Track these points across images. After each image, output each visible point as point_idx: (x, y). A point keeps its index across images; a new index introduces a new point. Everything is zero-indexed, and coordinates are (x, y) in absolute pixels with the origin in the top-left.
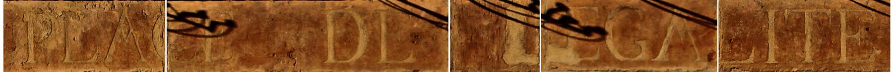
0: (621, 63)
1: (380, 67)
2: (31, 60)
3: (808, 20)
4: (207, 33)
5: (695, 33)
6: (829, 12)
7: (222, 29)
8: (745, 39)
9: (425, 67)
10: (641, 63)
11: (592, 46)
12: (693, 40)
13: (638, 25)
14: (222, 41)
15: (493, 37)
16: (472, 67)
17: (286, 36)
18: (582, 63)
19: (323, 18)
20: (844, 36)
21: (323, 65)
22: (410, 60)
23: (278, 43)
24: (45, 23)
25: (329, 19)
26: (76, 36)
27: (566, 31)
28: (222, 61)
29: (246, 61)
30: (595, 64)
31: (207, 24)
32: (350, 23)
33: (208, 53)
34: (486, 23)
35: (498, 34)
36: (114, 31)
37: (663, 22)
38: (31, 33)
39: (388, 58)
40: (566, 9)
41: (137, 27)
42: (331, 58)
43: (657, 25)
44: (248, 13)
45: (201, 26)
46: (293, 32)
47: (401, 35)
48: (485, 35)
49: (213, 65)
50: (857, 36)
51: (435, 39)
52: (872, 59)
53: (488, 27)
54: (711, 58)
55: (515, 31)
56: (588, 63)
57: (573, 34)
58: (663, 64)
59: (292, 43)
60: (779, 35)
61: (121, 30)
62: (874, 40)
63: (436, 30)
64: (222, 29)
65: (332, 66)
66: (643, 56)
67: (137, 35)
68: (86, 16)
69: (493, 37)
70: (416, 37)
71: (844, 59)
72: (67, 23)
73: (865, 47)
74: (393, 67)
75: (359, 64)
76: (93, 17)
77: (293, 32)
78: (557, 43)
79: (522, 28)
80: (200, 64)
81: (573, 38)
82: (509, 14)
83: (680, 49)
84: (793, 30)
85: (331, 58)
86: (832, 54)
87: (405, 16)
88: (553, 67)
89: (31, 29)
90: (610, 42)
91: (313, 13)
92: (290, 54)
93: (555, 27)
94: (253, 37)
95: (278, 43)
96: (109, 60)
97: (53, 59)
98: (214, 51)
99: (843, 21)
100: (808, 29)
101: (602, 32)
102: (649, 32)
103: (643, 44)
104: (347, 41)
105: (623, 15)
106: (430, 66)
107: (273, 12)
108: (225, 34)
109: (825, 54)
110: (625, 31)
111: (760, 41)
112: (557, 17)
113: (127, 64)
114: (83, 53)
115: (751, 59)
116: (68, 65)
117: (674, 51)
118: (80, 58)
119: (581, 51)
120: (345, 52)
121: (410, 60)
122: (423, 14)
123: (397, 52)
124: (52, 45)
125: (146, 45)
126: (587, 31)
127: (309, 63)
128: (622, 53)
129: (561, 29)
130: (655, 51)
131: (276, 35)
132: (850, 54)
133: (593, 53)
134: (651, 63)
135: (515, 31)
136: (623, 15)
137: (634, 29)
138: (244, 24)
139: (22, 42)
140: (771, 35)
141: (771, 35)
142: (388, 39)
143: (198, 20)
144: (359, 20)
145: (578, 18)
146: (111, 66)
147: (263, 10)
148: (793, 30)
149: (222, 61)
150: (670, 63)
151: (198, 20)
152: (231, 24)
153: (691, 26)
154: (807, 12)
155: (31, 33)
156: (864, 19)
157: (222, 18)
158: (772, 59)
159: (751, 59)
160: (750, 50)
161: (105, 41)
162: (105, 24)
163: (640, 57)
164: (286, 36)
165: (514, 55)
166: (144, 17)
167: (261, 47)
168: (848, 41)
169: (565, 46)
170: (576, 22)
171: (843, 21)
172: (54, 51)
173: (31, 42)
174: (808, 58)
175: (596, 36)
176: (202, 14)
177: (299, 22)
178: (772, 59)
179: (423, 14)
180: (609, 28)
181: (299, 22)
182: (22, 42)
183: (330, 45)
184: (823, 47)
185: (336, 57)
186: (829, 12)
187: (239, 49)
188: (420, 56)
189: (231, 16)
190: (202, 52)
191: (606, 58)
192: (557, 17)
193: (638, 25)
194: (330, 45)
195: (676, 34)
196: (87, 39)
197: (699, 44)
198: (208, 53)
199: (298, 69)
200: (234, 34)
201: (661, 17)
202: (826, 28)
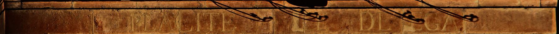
0: (430, 32)
1: (379, 32)
2: (133, 30)
3: (211, 16)
4: (318, 20)
5: (456, 21)
6: (218, 14)
7: (323, 19)
8: (189, 23)
9: (395, 32)
10: (437, 31)
11: (419, 25)
12: (455, 23)
13: (436, 18)
14: (323, 23)
15: (288, 22)
16: (280, 32)
17: (346, 21)
18: (416, 31)
19: (359, 15)
20: (224, 22)
21: (359, 31)
22: (389, 29)
23: (343, 23)
24: (137, 17)
25: (361, 15)
26: (148, 22)
27: (410, 20)
28: (323, 30)
29: (332, 30)
30: (421, 32)
31: (318, 17)
32: (368, 16)
33: (318, 27)
34: (285, 17)
35: (289, 21)
36: (162, 20)
37: (445, 17)
38: (133, 21)
39: (382, 29)
40: (410, 13)
41: (170, 19)
42: (361, 29)
43: (442, 18)
44: (333, 13)
45: (316, 18)
46: (348, 20)
47: (386, 21)
48: (285, 22)
49: (320, 31)
50: (228, 22)
51: (398, 22)
52: (234, 30)
53: (286, 19)
54: (461, 29)
55: (295, 20)
56: (418, 32)
57: (413, 21)
58: (444, 32)
59: (348, 24)
60: (201, 22)
61: (164, 19)
62: (234, 23)
63: (399, 19)
64: (323, 19)
65: (362, 31)
66: (437, 29)
67: (170, 21)
68: (152, 14)
69: (288, 22)
70: (391, 21)
71: (224, 30)
72: (145, 17)
73: (231, 26)
74: (383, 32)
75: (372, 31)
76: (154, 15)
77: (348, 20)
78: (407, 24)
79: (298, 19)
80: (316, 31)
81: (413, 23)
82: (293, 14)
83: (451, 27)
84: (206, 20)
85: (361, 29)
86: (220, 28)
87: (388, 14)
88: (406, 33)
89: (133, 19)
90: (426, 24)
91: (355, 13)
92: (347, 27)
93: (406, 19)
94: (334, 21)
95: (343, 23)
96: (160, 30)
97: (140, 30)
98: (321, 26)
99: (223, 17)
100: (211, 20)
101: (423, 21)
102: (439, 20)
103: (437, 25)
104: (367, 23)
105: (430, 15)
106: (396, 31)
107: (341, 13)
108: (324, 20)
109: (217, 28)
110: (431, 20)
111: (194, 24)
112: (407, 15)
113: (166, 31)
114: (151, 27)
115: (191, 30)
116: (146, 31)
117: (448, 27)
118: (150, 29)
119: (416, 27)
120: (367, 27)
121: (389, 29)
122: (394, 13)
123: (385, 26)
124: (140, 25)
125: (173, 25)
126: (418, 20)
127: (354, 31)
128: (430, 28)
129: (408, 20)
130: (441, 27)
131: (342, 21)
132: (226, 28)
133: (420, 28)
134: (440, 31)
135: (295, 20)
136: (430, 15)
137: (434, 20)
138: (331, 17)
139: (130, 24)
140: (198, 22)
141: (198, 22)
142: (382, 22)
143: (315, 16)
144: (372, 16)
145: (414, 16)
146: (161, 32)
147: (338, 12)
148: (206, 20)
149: (323, 30)
150: (447, 31)
151: (315, 16)
152: (326, 17)
153: (454, 18)
154: (211, 14)
155: (133, 21)
156: (231, 16)
157: (323, 15)
158: (198, 30)
159: (191, 30)
160: (191, 27)
161: (159, 23)
162: (159, 17)
163: (436, 29)
164: (346, 21)
165: (295, 28)
166: (172, 15)
167: (337, 25)
168: (225, 24)
169: (410, 26)
170: (414, 17)
171: (223, 17)
172: (141, 27)
173: (133, 23)
174: (211, 30)
175: (421, 22)
176: (316, 14)
177: (350, 16)
178: (198, 30)
179: (394, 13)
180: (425, 19)
181: (350, 16)
182: (130, 24)
183: (361, 24)
184: (216, 26)
185: (363, 28)
186: (218, 14)
187: (329, 26)
188: (393, 28)
189: (327, 14)
190: (316, 27)
191: (424, 30)
192: (407, 15)
193: (436, 18)
194: (361, 24)
195: (449, 21)
196: (153, 23)
197: (457, 25)
198: (318, 27)
199: (350, 32)
200: (327, 20)
201: (444, 15)
202: (218, 20)
